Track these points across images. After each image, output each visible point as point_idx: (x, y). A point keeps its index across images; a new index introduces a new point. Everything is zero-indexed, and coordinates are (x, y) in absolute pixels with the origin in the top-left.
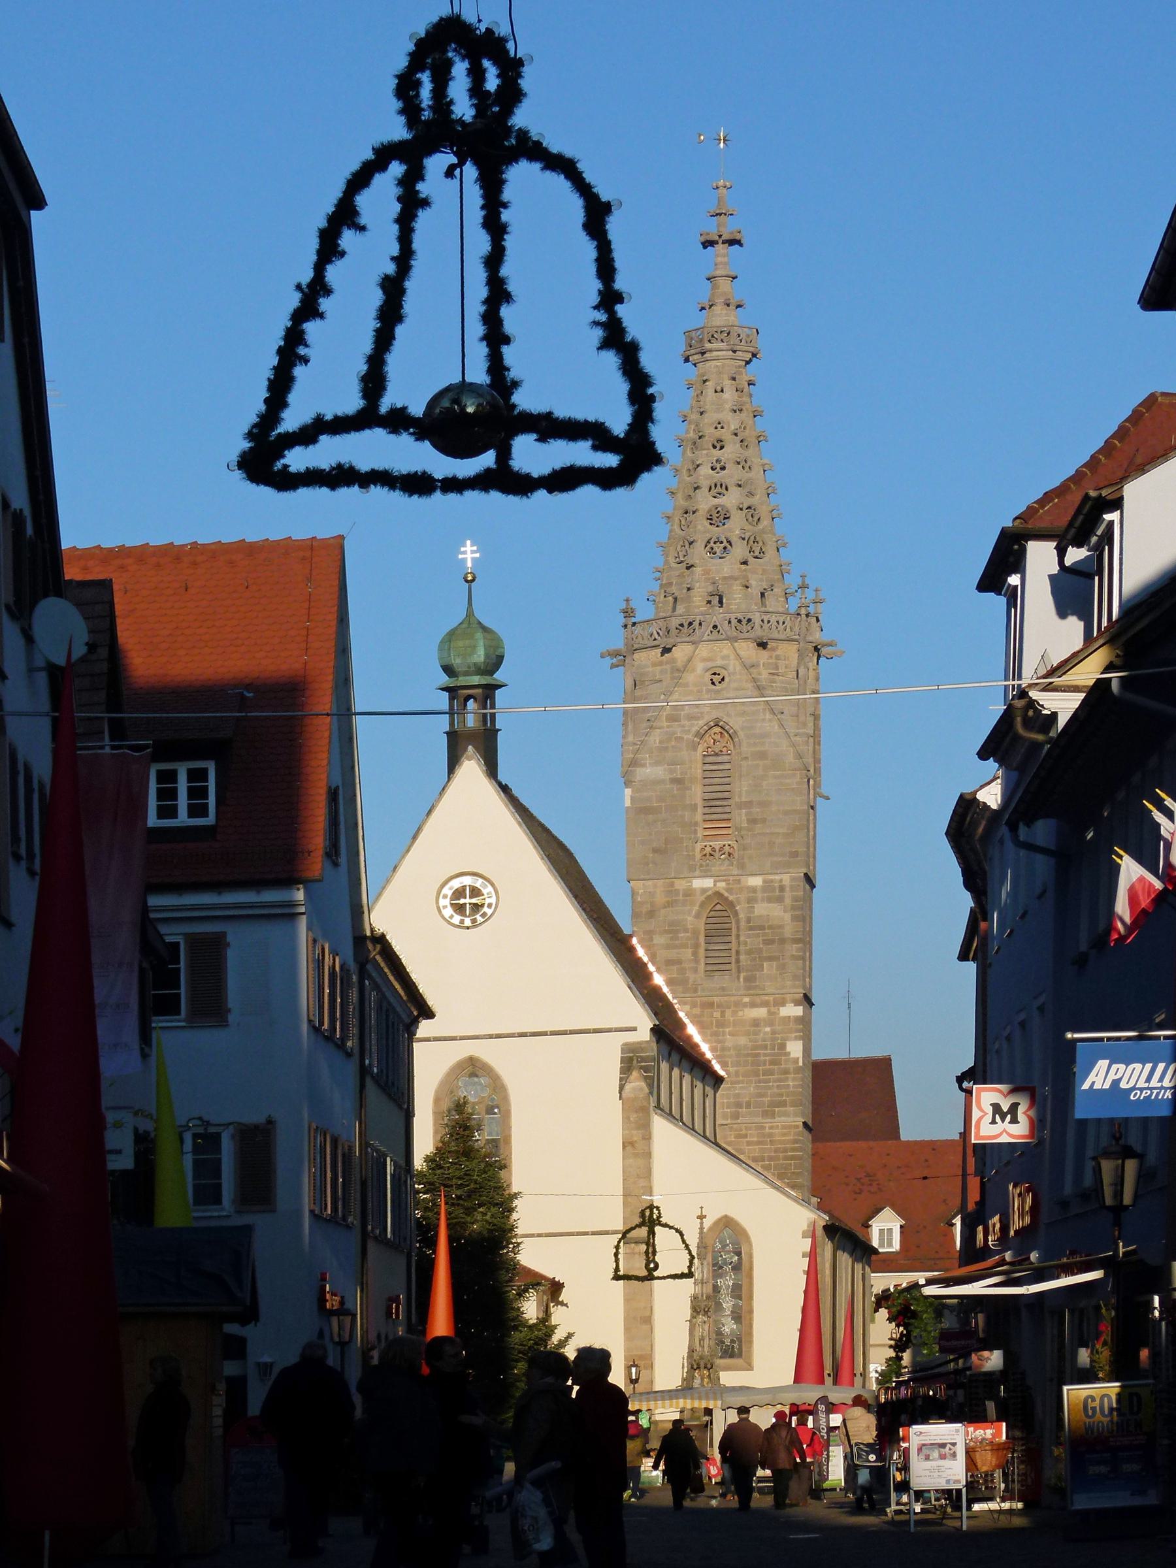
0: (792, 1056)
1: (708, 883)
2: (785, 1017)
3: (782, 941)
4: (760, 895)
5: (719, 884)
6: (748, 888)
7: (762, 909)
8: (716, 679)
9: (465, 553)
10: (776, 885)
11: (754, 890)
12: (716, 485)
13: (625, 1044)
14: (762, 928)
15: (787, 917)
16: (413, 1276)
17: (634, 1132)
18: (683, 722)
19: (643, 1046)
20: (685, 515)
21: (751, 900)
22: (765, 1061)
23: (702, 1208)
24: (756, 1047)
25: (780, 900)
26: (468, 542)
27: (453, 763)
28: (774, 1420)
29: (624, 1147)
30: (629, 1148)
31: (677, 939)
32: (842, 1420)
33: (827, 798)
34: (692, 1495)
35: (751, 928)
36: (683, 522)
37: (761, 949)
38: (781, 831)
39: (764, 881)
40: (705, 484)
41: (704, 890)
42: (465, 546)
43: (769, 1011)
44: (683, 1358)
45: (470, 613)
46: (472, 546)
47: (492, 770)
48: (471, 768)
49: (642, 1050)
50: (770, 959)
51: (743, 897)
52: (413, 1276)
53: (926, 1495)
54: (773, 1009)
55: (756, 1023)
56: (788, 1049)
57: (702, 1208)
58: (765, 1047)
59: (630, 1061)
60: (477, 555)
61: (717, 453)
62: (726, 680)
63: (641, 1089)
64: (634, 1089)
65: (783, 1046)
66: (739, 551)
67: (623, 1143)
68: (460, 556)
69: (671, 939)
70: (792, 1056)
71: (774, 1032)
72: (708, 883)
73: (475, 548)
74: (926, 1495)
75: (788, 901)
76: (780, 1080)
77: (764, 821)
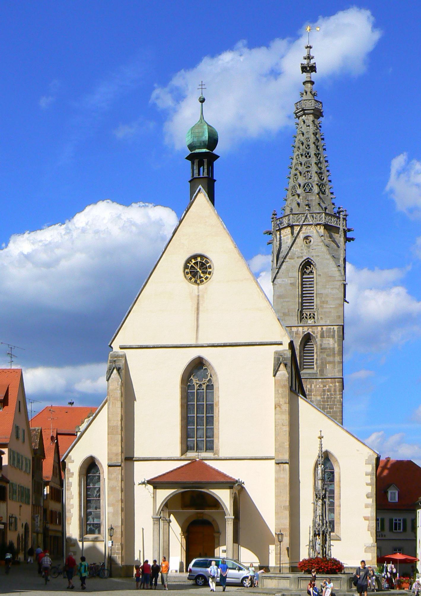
8: (308, 241)
10: (332, 330)
12: (307, 163)
17: (281, 399)
20: (295, 176)
23: (321, 431)
27: (192, 192)
28: (72, 459)
29: (275, 408)
30: (278, 409)
33: (348, 303)
34: (113, 476)
36: (295, 179)
44: (310, 527)
45: (202, 117)
47: (212, 197)
48: (202, 198)
50: (330, 363)
53: (97, 531)
57: (321, 431)
63: (284, 375)
64: (280, 374)
67: (275, 406)
74: (97, 531)
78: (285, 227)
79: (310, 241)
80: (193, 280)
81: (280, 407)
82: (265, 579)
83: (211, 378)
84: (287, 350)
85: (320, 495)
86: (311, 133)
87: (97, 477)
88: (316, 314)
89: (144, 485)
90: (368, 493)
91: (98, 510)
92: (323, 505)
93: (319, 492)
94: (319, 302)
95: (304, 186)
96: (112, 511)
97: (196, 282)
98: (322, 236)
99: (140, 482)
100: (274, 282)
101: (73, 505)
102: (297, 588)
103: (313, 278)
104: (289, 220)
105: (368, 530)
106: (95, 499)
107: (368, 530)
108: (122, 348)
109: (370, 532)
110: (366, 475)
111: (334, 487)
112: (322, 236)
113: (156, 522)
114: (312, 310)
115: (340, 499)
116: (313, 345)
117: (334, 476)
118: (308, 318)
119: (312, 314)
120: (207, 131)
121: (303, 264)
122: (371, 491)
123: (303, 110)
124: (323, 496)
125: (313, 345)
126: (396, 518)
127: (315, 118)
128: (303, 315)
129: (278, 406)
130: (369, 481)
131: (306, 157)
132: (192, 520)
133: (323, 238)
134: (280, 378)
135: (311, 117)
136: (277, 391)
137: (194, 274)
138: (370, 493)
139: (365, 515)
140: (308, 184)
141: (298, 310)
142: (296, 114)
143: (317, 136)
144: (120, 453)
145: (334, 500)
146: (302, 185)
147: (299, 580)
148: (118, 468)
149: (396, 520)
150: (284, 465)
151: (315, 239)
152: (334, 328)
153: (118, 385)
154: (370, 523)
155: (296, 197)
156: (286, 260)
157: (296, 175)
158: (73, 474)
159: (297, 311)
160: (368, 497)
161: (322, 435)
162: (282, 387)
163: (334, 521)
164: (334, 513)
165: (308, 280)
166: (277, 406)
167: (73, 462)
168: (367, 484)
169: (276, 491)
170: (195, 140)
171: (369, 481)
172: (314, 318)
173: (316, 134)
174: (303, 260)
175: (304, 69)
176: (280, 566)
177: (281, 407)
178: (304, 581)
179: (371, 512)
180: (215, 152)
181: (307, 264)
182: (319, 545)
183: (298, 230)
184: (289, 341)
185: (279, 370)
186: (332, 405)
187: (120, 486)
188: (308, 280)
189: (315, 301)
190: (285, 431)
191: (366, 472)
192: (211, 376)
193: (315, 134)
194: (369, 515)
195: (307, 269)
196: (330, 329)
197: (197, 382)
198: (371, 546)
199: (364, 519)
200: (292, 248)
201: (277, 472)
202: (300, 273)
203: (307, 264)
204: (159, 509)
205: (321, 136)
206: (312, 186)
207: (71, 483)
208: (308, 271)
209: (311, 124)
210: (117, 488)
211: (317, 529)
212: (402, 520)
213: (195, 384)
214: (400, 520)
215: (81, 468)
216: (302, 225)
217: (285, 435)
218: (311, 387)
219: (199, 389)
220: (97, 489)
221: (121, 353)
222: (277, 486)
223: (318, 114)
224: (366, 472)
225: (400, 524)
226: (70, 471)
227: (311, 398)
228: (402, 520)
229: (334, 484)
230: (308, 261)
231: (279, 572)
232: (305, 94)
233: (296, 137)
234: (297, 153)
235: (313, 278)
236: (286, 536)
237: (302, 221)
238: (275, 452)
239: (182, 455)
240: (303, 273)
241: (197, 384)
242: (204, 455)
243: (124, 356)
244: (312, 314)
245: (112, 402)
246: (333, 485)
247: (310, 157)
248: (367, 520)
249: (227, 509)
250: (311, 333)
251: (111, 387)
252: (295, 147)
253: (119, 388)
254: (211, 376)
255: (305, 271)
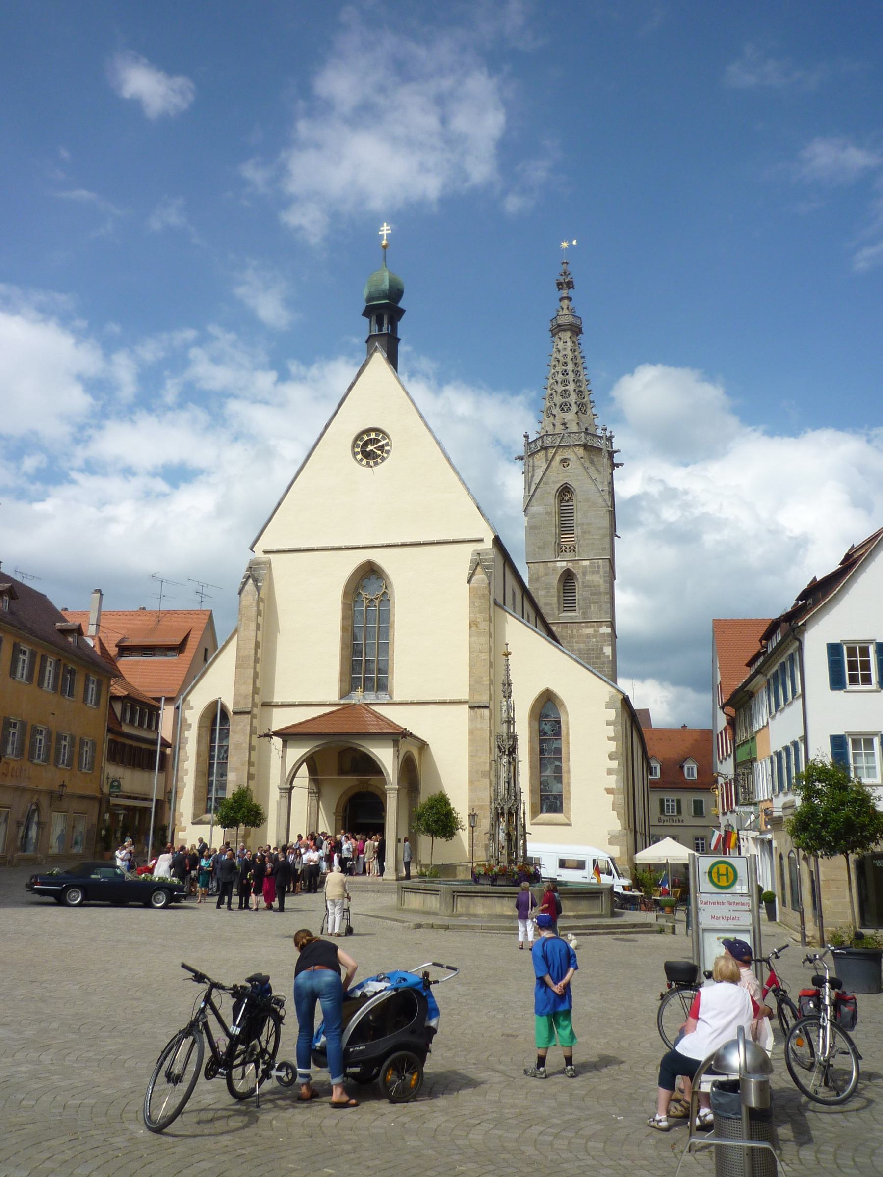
0: (606, 654)
1: (564, 564)
2: (602, 634)
3: (600, 593)
4: (588, 570)
5: (569, 564)
6: (582, 566)
7: (590, 577)
8: (565, 464)
9: (383, 230)
10: (596, 565)
11: (585, 567)
13: (475, 551)
14: (590, 587)
15: (602, 581)
16: (189, 689)
17: (478, 615)
18: (551, 485)
19: (487, 551)
21: (584, 572)
22: (593, 657)
24: (589, 649)
25: (598, 572)
26: (385, 224)
30: (474, 628)
31: (550, 592)
32: (224, 984)
33: (619, 537)
35: (585, 587)
37: (590, 598)
38: (597, 537)
39: (590, 563)
40: (559, 381)
41: (562, 567)
42: (383, 226)
43: (594, 631)
46: (387, 226)
48: (379, 359)
49: (487, 554)
50: (595, 603)
51: (580, 571)
52: (189, 689)
54: (596, 629)
55: (588, 636)
56: (604, 651)
58: (593, 650)
59: (477, 564)
60: (390, 231)
61: (564, 368)
62: (570, 465)
63: (483, 580)
65: (602, 649)
66: (574, 409)
68: (380, 233)
69: (547, 592)
70: (606, 654)
71: (597, 642)
72: (564, 564)
73: (389, 228)
75: (602, 573)
76: (600, 667)
77: (589, 532)
78: (539, 451)
79: (568, 465)
80: (365, 461)
81: (477, 626)
82: (407, 892)
83: (386, 590)
84: (490, 549)
85: (504, 748)
86: (569, 349)
87: (226, 731)
88: (576, 547)
89: (267, 739)
90: (611, 752)
91: (224, 778)
92: (509, 763)
93: (503, 741)
94: (580, 531)
95: (561, 406)
96: (235, 779)
97: (368, 464)
98: (582, 458)
99: (262, 734)
100: (527, 512)
101: (187, 770)
102: (450, 911)
103: (573, 506)
104: (543, 442)
105: (613, 810)
106: (222, 761)
107: (613, 810)
108: (266, 552)
109: (615, 813)
110: (607, 725)
111: (561, 744)
112: (582, 458)
113: (284, 795)
114: (573, 542)
115: (569, 761)
116: (574, 583)
117: (560, 727)
118: (568, 551)
119: (572, 547)
120: (388, 278)
121: (560, 490)
122: (616, 749)
123: (559, 326)
124: (511, 750)
125: (574, 583)
126: (668, 798)
127: (573, 334)
128: (561, 548)
129: (474, 624)
130: (612, 735)
131: (563, 374)
132: (353, 792)
133: (582, 460)
134: (476, 585)
135: (569, 334)
136: (472, 603)
137: (368, 455)
138: (614, 752)
139: (608, 787)
140: (566, 404)
141: (555, 542)
142: (552, 331)
143: (576, 353)
144: (251, 695)
145: (561, 763)
146: (558, 405)
147: (454, 896)
148: (246, 716)
149: (668, 801)
150: (482, 710)
151: (574, 463)
152: (598, 562)
153: (254, 600)
154: (616, 798)
155: (552, 417)
156: (540, 486)
157: (552, 395)
158: (190, 725)
159: (553, 543)
160: (611, 759)
161: (509, 650)
162: (479, 598)
163: (562, 795)
164: (562, 783)
165: (567, 508)
166: (473, 624)
167: (191, 708)
168: (610, 739)
169: (471, 748)
170: (373, 290)
171: (612, 735)
172: (574, 551)
173: (575, 351)
174: (559, 485)
175: (560, 286)
176: (473, 866)
177: (478, 625)
178: (463, 898)
179: (617, 781)
180: (401, 305)
181: (565, 491)
182: (504, 832)
183: (554, 452)
184: (494, 537)
185: (476, 574)
186: (599, 653)
187: (248, 742)
188: (567, 508)
189: (575, 530)
190: (484, 660)
191: (607, 721)
192: (386, 588)
193: (573, 351)
194: (614, 786)
195: (565, 495)
196: (594, 563)
197: (367, 597)
198: (617, 834)
199: (606, 792)
200: (548, 472)
201: (471, 720)
202: (556, 500)
203: (565, 491)
204: (289, 775)
205: (580, 352)
206: (571, 406)
207: (187, 738)
208: (566, 498)
209: (568, 340)
210: (244, 745)
211: (499, 804)
212: (675, 801)
213: (364, 600)
214: (673, 801)
215: (203, 717)
216: (558, 446)
217: (484, 666)
218: (572, 631)
219: (369, 606)
220: (226, 748)
221: (264, 560)
222: (472, 741)
223: (577, 330)
224: (607, 721)
225: (673, 805)
226: (187, 722)
227: (573, 646)
228: (675, 801)
229: (560, 739)
230: (566, 487)
231: (738, 856)
232: (561, 310)
233: (552, 356)
234: (553, 371)
235: (573, 506)
236: (485, 818)
237: (558, 443)
238: (470, 691)
239: (341, 698)
240: (562, 500)
241: (367, 599)
242: (371, 697)
243: (269, 564)
244: (572, 547)
245: (245, 623)
246: (558, 742)
247: (567, 374)
248: (611, 794)
249: (388, 774)
250: (571, 568)
251: (244, 603)
252: (550, 366)
253: (254, 605)
254: (386, 588)
255: (563, 499)
